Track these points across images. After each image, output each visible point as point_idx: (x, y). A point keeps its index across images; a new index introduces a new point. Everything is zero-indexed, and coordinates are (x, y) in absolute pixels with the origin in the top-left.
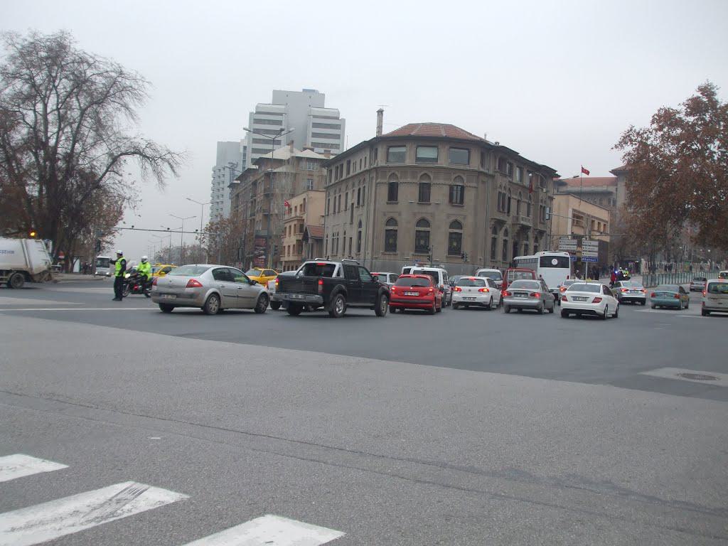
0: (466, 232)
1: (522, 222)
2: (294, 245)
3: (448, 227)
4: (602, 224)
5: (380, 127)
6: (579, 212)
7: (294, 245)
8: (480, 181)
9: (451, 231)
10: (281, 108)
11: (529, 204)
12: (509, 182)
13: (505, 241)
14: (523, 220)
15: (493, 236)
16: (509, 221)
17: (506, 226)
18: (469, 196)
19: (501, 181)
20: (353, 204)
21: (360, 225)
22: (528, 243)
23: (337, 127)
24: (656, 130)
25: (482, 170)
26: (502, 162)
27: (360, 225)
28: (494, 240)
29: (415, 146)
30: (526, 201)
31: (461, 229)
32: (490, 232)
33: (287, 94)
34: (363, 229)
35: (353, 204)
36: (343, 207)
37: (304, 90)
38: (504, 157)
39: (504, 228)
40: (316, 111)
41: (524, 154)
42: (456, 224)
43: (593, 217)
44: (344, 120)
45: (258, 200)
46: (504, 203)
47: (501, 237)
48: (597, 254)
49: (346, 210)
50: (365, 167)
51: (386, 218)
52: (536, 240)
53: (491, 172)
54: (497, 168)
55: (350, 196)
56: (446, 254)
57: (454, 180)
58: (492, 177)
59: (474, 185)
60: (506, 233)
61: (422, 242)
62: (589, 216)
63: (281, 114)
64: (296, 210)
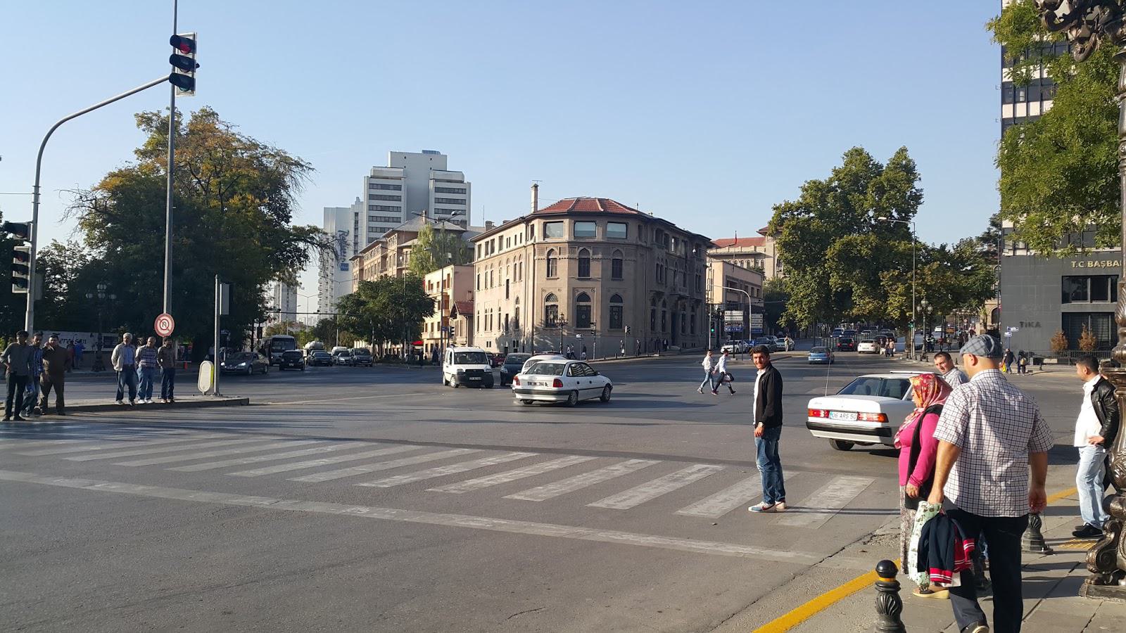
0: (627, 304)
1: (679, 293)
2: (439, 323)
3: (609, 301)
4: (756, 288)
5: (536, 207)
6: (733, 278)
7: (439, 323)
8: (639, 255)
9: (612, 304)
10: (399, 172)
11: (685, 274)
12: (666, 253)
13: (664, 312)
14: (680, 290)
15: (653, 307)
16: (667, 292)
17: (665, 297)
18: (627, 269)
19: (659, 253)
20: (508, 280)
21: (517, 301)
22: (685, 313)
23: (463, 191)
24: (803, 277)
25: (640, 243)
26: (659, 232)
27: (517, 301)
28: (653, 312)
29: (573, 221)
30: (673, 268)
31: (622, 302)
32: (649, 303)
33: (405, 156)
34: (521, 306)
35: (508, 280)
36: (496, 282)
37: (424, 151)
38: (662, 229)
39: (662, 300)
40: (440, 175)
41: (680, 225)
42: (616, 298)
43: (747, 282)
44: (470, 184)
45: (366, 268)
46: (660, 272)
47: (659, 308)
48: (742, 317)
49: (500, 285)
50: (521, 242)
51: (545, 295)
52: (693, 310)
53: (649, 245)
54: (654, 239)
55: (504, 271)
56: (608, 328)
57: (613, 255)
58: (649, 249)
59: (633, 258)
60: (664, 305)
61: (583, 317)
62: (741, 281)
63: (692, 332)
64: (438, 287)
